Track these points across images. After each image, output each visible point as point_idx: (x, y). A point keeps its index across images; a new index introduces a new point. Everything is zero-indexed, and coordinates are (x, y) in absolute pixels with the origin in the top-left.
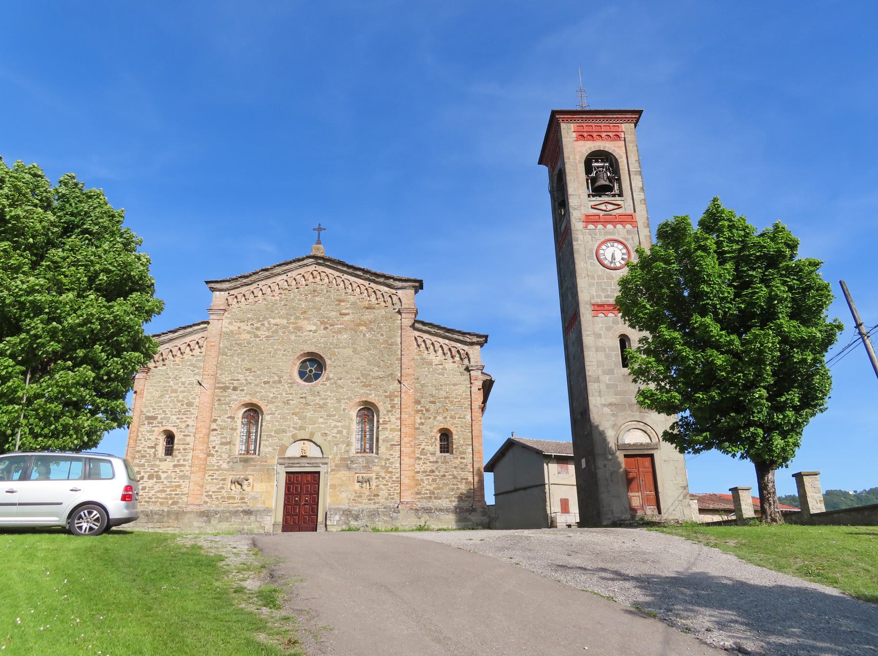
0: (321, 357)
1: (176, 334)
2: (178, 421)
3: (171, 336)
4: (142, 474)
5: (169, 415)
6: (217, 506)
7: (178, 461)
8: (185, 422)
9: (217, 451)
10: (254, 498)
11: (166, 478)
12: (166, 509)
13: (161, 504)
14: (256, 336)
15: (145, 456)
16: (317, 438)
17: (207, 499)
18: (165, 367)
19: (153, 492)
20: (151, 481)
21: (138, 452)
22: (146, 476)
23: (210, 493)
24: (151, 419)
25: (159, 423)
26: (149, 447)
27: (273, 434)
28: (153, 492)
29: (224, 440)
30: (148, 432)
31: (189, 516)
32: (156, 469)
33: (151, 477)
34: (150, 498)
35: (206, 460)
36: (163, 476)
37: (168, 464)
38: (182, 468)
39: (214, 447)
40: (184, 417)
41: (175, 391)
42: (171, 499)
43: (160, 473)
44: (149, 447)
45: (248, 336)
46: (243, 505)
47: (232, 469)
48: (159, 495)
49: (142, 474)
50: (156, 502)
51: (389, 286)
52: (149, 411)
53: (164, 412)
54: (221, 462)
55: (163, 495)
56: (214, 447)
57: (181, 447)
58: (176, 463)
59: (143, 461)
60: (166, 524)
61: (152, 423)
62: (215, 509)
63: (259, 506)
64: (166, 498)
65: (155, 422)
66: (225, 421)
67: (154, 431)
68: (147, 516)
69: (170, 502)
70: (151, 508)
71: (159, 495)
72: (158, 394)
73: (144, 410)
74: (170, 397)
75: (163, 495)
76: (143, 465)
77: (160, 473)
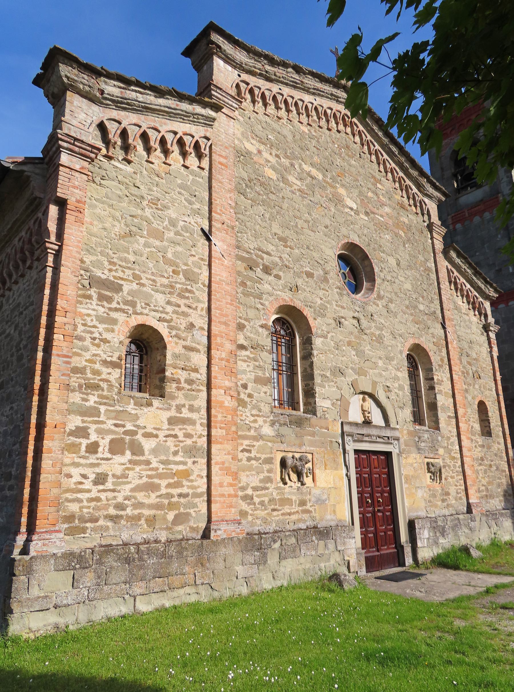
0: (365, 257)
1: (161, 101)
2: (169, 309)
3: (150, 99)
4: (93, 437)
5: (147, 289)
6: (265, 521)
7: (179, 408)
8: (185, 315)
9: (250, 396)
10: (319, 501)
11: (155, 451)
12: (163, 536)
13: (151, 521)
14: (285, 180)
15: (97, 387)
16: (382, 397)
17: (244, 506)
18: (128, 169)
19: (126, 490)
20: (118, 459)
21: (76, 370)
22: (104, 443)
23: (249, 492)
24: (107, 288)
25: (126, 303)
26: (105, 363)
27: (328, 374)
28: (126, 490)
29: (260, 374)
30: (101, 320)
31: (223, 551)
32: (129, 427)
33: (116, 447)
34: (120, 507)
35: (235, 410)
36: (148, 445)
37: (153, 415)
38: (189, 429)
39: (245, 386)
40: (182, 302)
41: (159, 235)
42: (171, 506)
43: (139, 437)
44: (105, 363)
45: (273, 175)
46: (306, 516)
47: (280, 437)
48: (141, 496)
49: (93, 437)
50: (138, 517)
51: (419, 186)
52: (99, 265)
53: (136, 277)
54: (260, 420)
55: (153, 498)
56: (245, 386)
57: (183, 375)
58: (173, 413)
59: (93, 400)
60: (176, 580)
61: (109, 300)
62: (262, 529)
63: (329, 517)
64: (158, 507)
65: (117, 297)
66: (257, 333)
67: (114, 322)
68: (128, 561)
69: (171, 516)
70: (125, 536)
71: (141, 496)
72: (119, 228)
73: (88, 259)
74: (146, 245)
75: (153, 498)
76: (94, 412)
77: (139, 437)
